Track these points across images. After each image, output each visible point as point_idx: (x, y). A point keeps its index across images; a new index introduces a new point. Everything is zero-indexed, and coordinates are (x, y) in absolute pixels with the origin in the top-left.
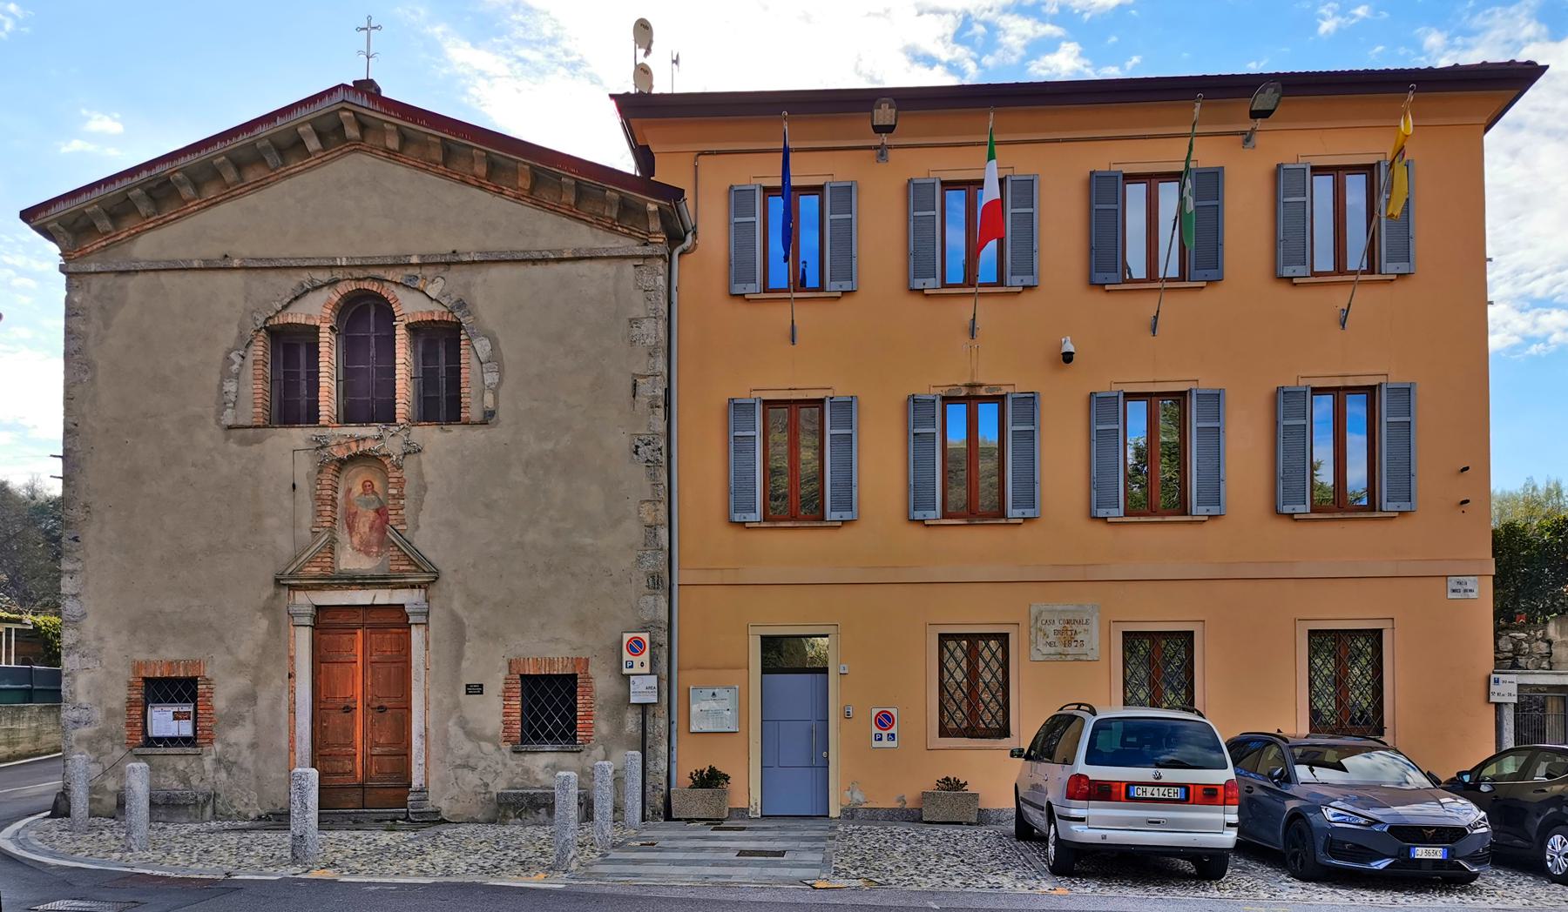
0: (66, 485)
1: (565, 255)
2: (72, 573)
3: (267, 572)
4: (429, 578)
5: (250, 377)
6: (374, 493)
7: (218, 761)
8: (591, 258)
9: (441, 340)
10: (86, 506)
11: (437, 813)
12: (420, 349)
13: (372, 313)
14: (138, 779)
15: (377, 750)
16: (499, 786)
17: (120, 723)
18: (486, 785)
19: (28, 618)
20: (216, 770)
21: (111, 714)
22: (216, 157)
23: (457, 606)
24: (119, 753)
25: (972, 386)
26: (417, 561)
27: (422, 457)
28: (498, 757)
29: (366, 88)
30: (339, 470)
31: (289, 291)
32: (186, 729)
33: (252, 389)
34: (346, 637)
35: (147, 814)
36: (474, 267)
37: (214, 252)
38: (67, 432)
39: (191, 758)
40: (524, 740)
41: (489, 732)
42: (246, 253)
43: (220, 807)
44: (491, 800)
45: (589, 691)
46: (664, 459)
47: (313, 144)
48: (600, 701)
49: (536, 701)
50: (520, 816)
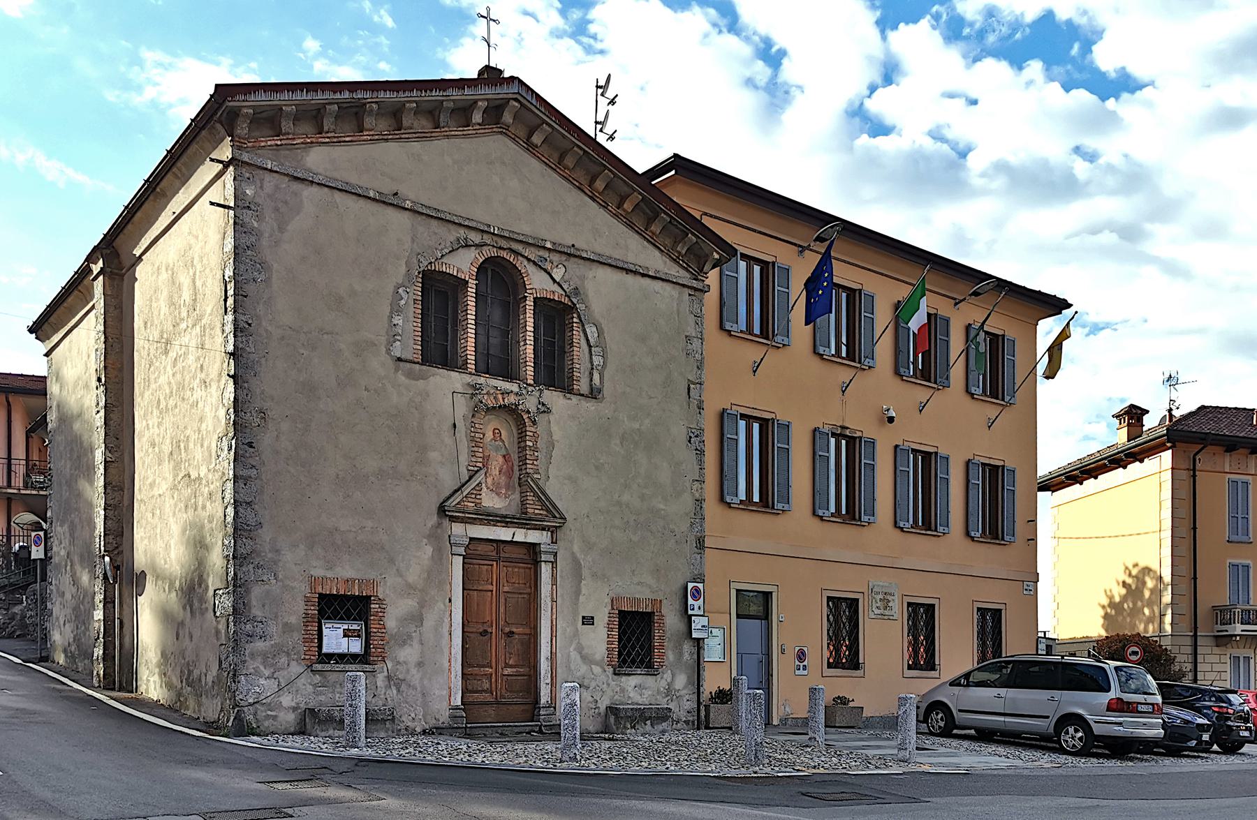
4: (552, 519)
7: (389, 678)
9: (558, 316)
17: (297, 636)
21: (287, 628)
23: (576, 548)
24: (296, 668)
25: (843, 428)
26: (551, 509)
27: (552, 417)
32: (356, 646)
36: (588, 263)
41: (598, 657)
47: (477, 117)
48: (668, 635)
50: (633, 727)
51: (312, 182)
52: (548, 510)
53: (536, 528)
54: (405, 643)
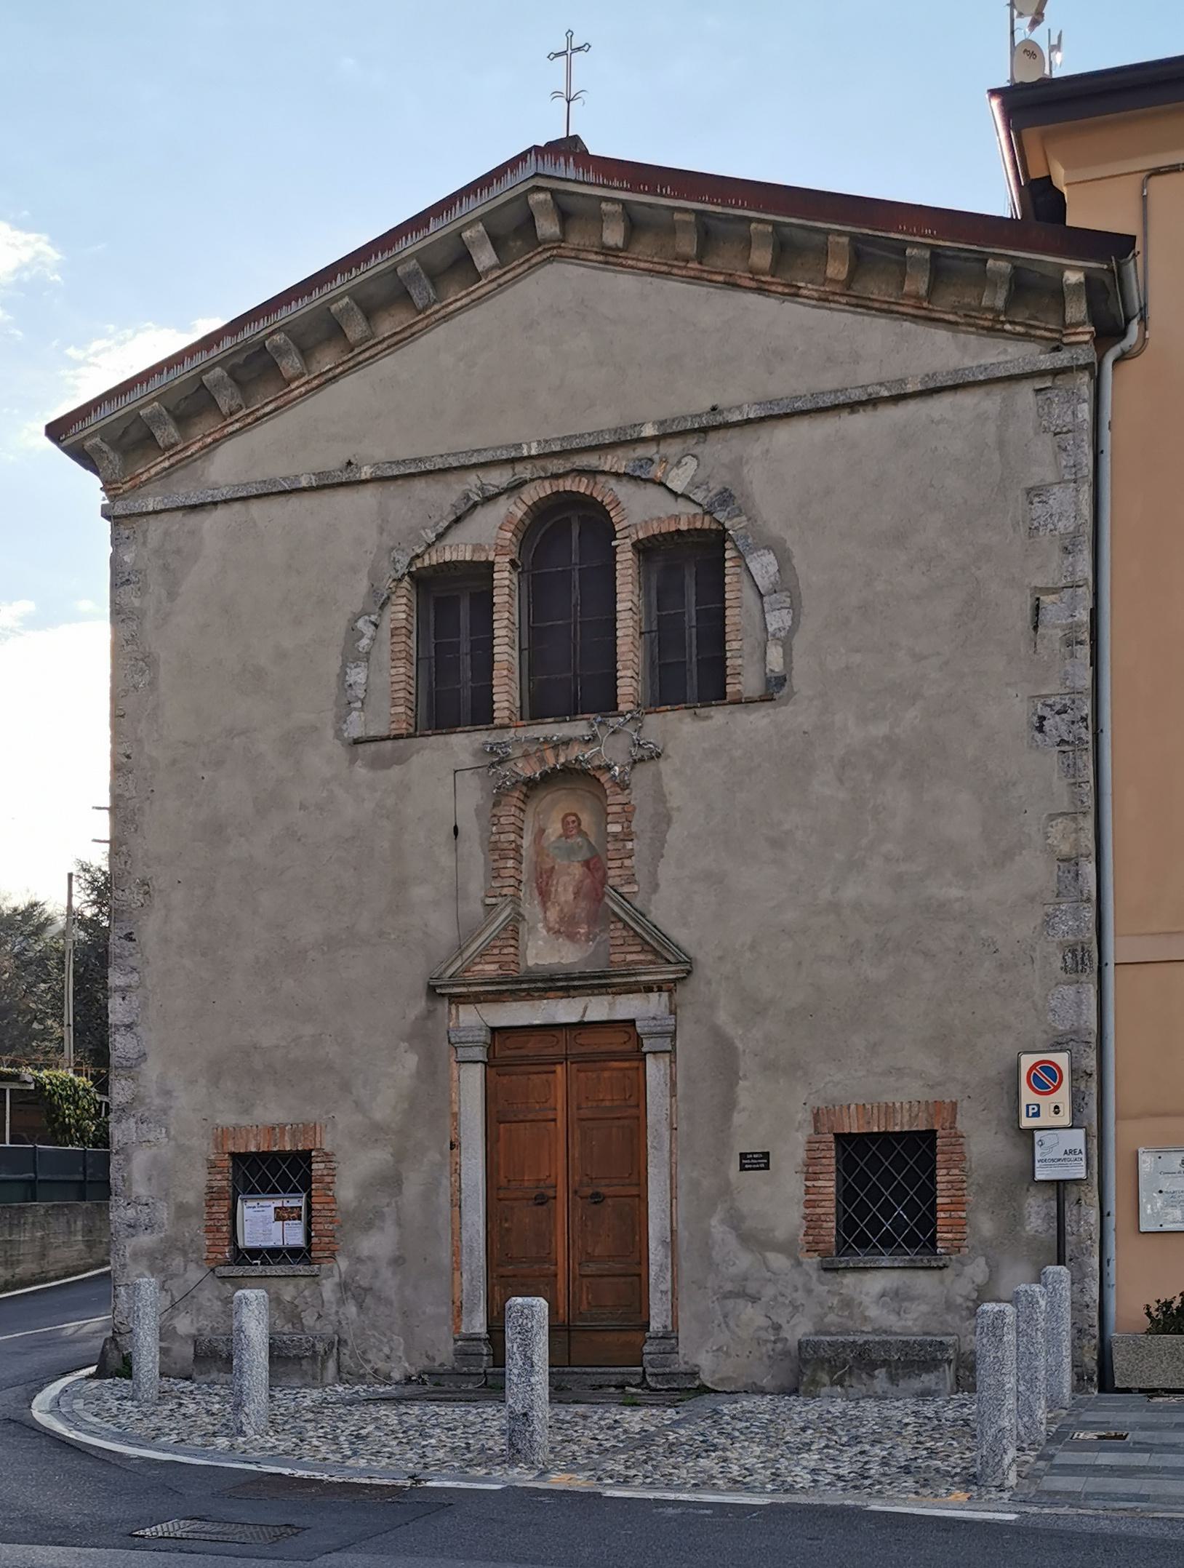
0: (114, 855)
1: (910, 388)
2: (124, 991)
3: (415, 974)
4: (673, 970)
5: (386, 656)
6: (581, 833)
7: (344, 1286)
8: (955, 388)
9: (694, 561)
10: (144, 883)
11: (694, 1375)
12: (654, 579)
13: (575, 533)
14: (254, 1317)
15: (592, 1269)
16: (799, 1329)
17: (195, 1229)
18: (777, 1328)
19: (28, 1073)
20: (341, 1302)
21: (182, 1211)
22: (335, 300)
24: (194, 1274)
26: (658, 946)
27: (663, 765)
29: (569, 148)
30: (526, 798)
31: (447, 509)
32: (294, 1235)
33: (388, 679)
35: (265, 1375)
36: (748, 430)
37: (330, 460)
38: (117, 769)
39: (303, 1282)
40: (843, 1248)
41: (781, 1234)
42: (380, 454)
43: (346, 1360)
44: (786, 1353)
45: (960, 1159)
46: (1088, 736)
47: (485, 258)
49: (862, 1180)
50: (840, 1382)
51: (215, 504)
52: (655, 952)
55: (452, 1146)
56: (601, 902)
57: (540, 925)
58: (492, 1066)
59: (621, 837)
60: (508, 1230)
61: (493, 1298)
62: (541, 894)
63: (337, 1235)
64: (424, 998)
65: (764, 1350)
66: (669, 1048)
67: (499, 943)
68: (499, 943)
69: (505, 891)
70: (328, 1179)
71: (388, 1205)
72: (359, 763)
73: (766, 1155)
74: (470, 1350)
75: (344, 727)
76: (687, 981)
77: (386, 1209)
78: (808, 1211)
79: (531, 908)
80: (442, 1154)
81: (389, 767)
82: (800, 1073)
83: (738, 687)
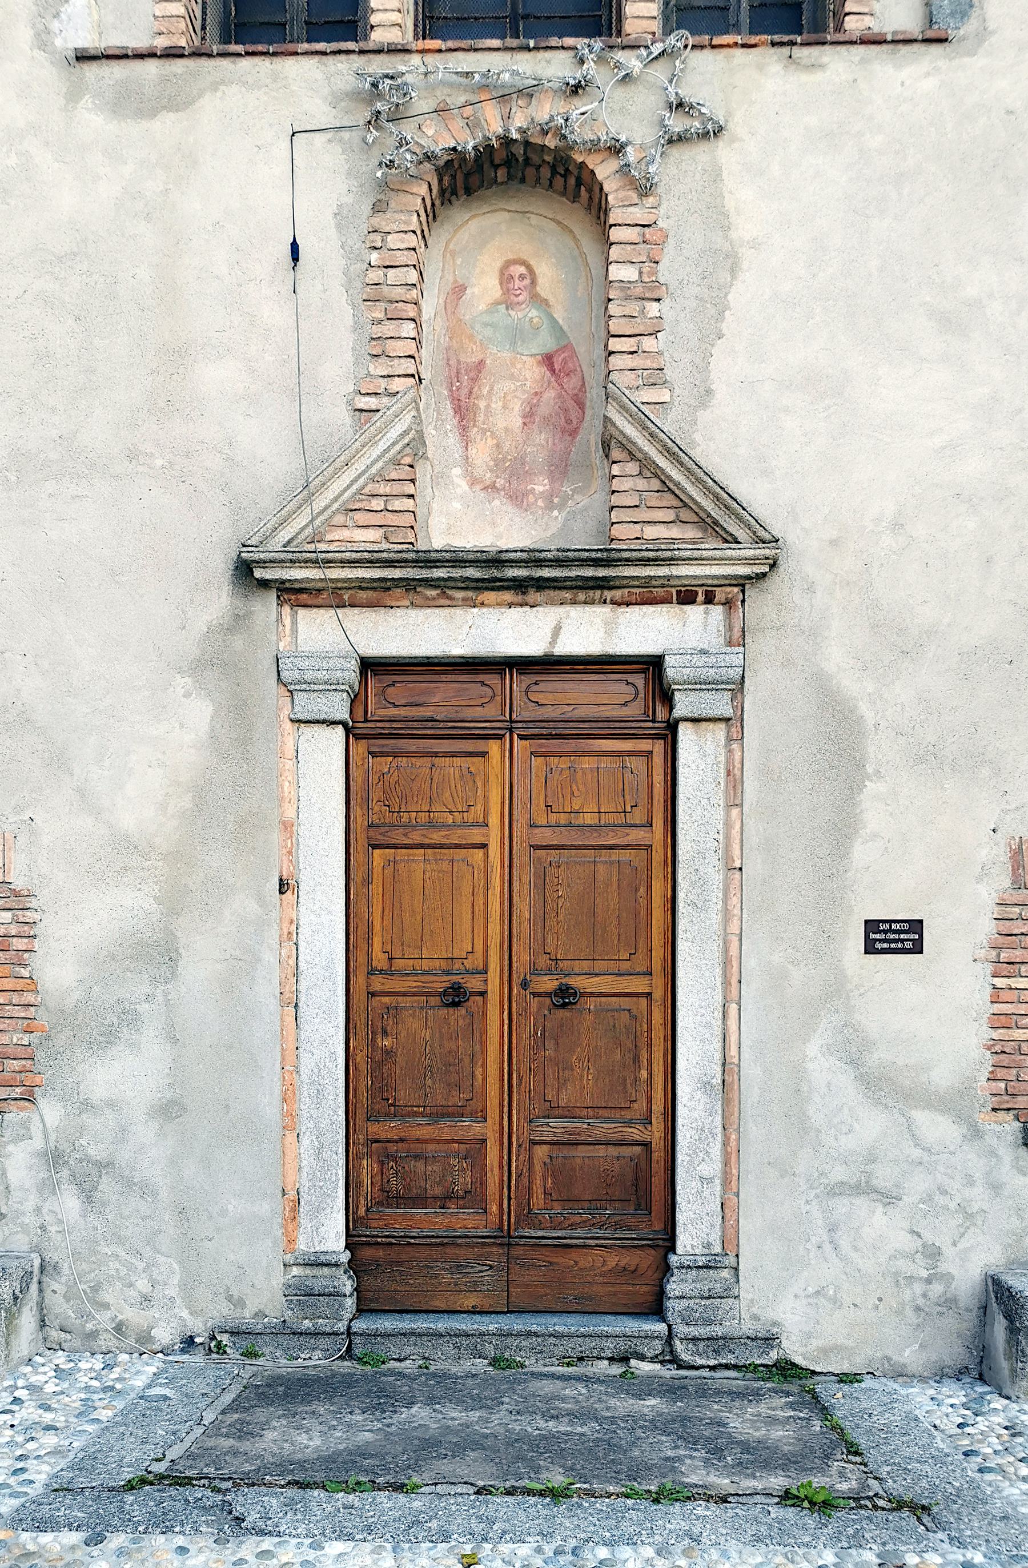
4: (723, 553)
6: (536, 299)
7: (53, 1159)
20: (49, 1188)
26: (715, 514)
27: (722, 151)
28: (973, 1160)
34: (451, 767)
41: (943, 1077)
43: (59, 1306)
44: (950, 1302)
53: (650, 595)
54: (110, 1037)
55: (283, 886)
56: (590, 417)
57: (457, 471)
58: (358, 737)
59: (638, 290)
60: (387, 1052)
61: (359, 1184)
62: (458, 410)
63: (40, 1055)
64: (226, 588)
65: (907, 1295)
66: (728, 712)
67: (383, 489)
68: (383, 489)
69: (397, 385)
70: (19, 944)
71: (148, 998)
72: (87, 101)
73: (916, 926)
74: (317, 1286)
75: (55, 25)
76: (767, 584)
77: (143, 1008)
78: (996, 1035)
79: (442, 438)
80: (261, 900)
81: (153, 113)
82: (985, 772)
83: (868, 21)
